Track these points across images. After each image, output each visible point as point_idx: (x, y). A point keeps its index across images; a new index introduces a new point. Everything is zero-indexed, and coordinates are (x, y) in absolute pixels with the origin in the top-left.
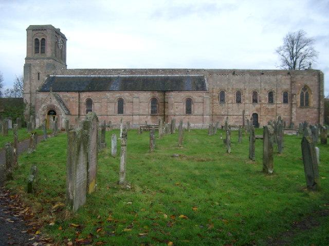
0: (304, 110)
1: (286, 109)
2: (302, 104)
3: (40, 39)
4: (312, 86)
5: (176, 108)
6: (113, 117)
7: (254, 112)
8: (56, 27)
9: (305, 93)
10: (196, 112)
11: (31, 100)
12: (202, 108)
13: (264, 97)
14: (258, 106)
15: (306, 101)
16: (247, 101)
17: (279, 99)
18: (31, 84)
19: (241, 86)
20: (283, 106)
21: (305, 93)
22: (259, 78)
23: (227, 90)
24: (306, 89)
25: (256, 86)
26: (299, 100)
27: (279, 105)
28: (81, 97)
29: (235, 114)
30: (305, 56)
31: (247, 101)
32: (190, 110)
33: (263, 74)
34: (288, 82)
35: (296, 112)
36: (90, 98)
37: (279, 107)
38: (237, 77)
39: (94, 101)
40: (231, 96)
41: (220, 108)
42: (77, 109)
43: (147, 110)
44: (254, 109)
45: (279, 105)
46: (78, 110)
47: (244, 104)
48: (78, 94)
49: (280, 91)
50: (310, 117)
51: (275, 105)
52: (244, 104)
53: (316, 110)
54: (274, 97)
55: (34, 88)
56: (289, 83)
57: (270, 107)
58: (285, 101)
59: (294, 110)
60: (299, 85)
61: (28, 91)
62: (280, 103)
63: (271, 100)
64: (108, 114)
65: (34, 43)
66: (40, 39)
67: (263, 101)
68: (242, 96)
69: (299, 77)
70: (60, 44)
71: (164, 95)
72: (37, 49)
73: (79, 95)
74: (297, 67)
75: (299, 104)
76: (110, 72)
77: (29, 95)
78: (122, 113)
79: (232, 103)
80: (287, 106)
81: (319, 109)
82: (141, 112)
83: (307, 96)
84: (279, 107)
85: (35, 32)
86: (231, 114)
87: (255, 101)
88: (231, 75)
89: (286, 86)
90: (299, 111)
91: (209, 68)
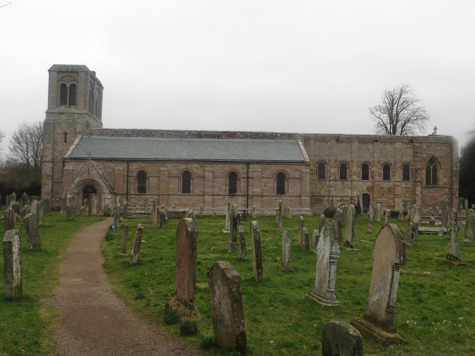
0: (431, 190)
1: (406, 188)
2: (428, 182)
3: (68, 85)
4: (442, 157)
5: (265, 186)
6: (176, 197)
7: (365, 192)
8: (91, 69)
9: (432, 167)
10: (291, 191)
11: (53, 172)
12: (299, 185)
13: (376, 170)
14: (368, 183)
15: (433, 177)
16: (355, 177)
17: (397, 176)
18: (54, 149)
19: (347, 158)
20: (403, 185)
21: (432, 167)
22: (370, 146)
23: (393, 165)
24: (433, 162)
25: (367, 157)
26: (424, 176)
27: (398, 184)
28: (131, 168)
29: (340, 195)
30: (408, 121)
31: (355, 177)
32: (283, 188)
33: (376, 141)
34: (410, 152)
35: (421, 192)
36: (143, 169)
37: (398, 186)
38: (343, 145)
39: (148, 175)
40: (333, 171)
41: (319, 186)
42: (125, 185)
43: (224, 188)
44: (365, 188)
45: (398, 184)
46: (125, 187)
47: (352, 181)
48: (126, 164)
49: (399, 165)
50: (440, 199)
51: (392, 183)
52: (352, 181)
53: (447, 190)
54: (391, 172)
55: (58, 154)
56: (411, 154)
57: (387, 185)
58: (406, 177)
59: (419, 189)
60: (425, 156)
61: (49, 158)
62: (400, 180)
63: (387, 177)
64: (170, 193)
65: (59, 90)
66: (68, 85)
67: (376, 178)
68: (348, 170)
69: (424, 146)
70: (96, 91)
71: (248, 168)
72: (63, 102)
73: (128, 164)
74: (398, 133)
75: (424, 182)
76: (154, 133)
77: (50, 165)
78: (189, 191)
79: (335, 180)
80: (409, 184)
81: (451, 189)
82: (216, 190)
83: (435, 170)
84: (398, 186)
85: (61, 75)
86: (334, 194)
87: (365, 177)
88: (334, 142)
89: (408, 158)
90: (425, 191)
91: (242, 131)
